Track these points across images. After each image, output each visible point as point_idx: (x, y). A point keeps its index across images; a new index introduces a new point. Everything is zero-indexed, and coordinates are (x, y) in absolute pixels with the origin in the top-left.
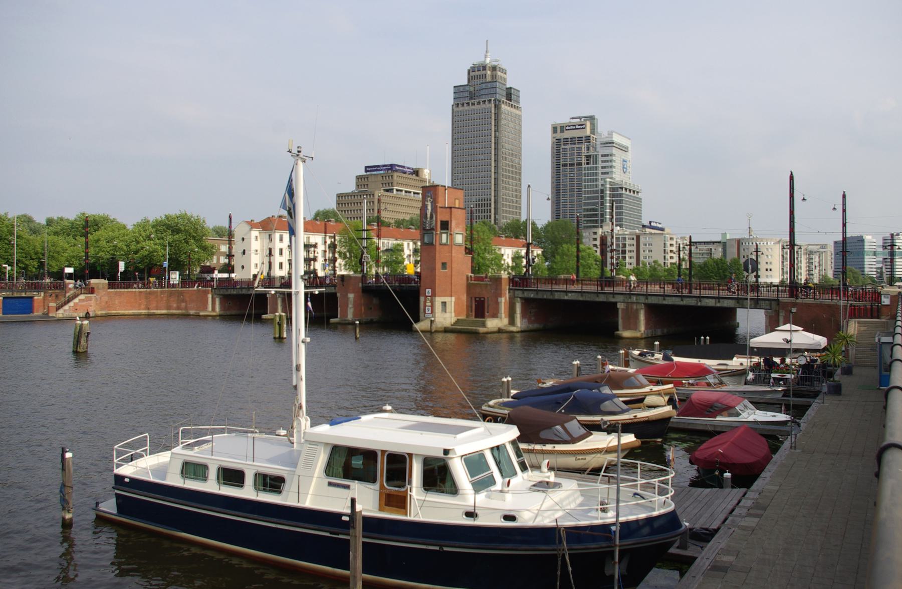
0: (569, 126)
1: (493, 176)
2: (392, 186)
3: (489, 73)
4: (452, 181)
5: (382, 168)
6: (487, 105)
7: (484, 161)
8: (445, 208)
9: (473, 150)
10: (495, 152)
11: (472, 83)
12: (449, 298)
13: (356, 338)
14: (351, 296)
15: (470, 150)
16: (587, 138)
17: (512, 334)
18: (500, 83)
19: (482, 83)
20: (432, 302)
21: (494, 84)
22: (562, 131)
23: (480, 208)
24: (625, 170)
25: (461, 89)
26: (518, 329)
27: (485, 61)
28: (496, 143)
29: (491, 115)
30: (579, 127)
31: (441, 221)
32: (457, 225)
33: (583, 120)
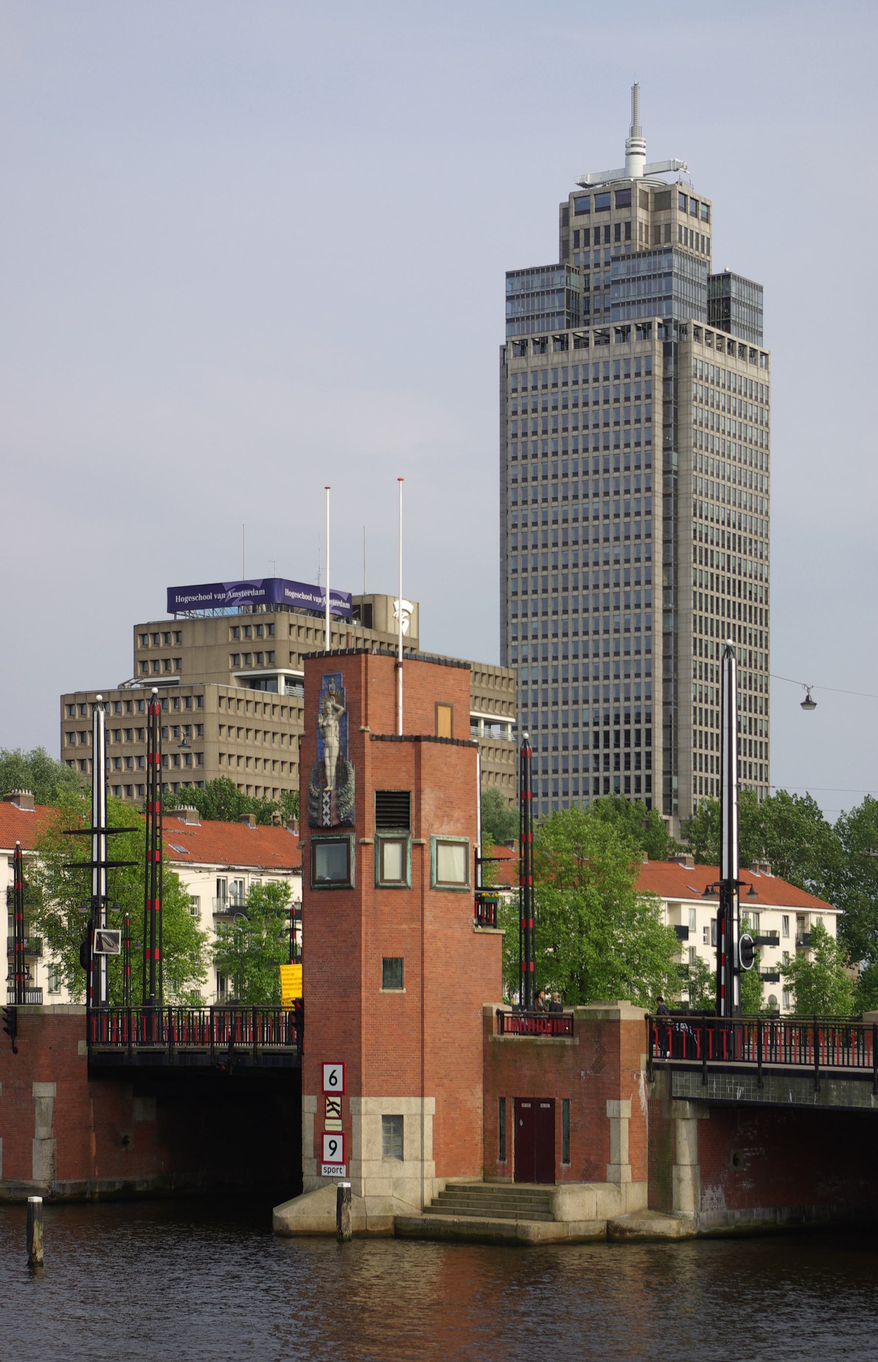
2: (273, 663)
3: (642, 216)
4: (504, 646)
5: (231, 595)
6: (636, 346)
8: (395, 739)
9: (581, 523)
10: (666, 531)
11: (579, 257)
12: (416, 1101)
13: (33, 1265)
14: (45, 1091)
15: (571, 525)
18: (683, 255)
19: (616, 259)
20: (347, 1116)
21: (663, 259)
25: (537, 283)
27: (627, 170)
28: (671, 496)
29: (650, 385)
32: (445, 808)
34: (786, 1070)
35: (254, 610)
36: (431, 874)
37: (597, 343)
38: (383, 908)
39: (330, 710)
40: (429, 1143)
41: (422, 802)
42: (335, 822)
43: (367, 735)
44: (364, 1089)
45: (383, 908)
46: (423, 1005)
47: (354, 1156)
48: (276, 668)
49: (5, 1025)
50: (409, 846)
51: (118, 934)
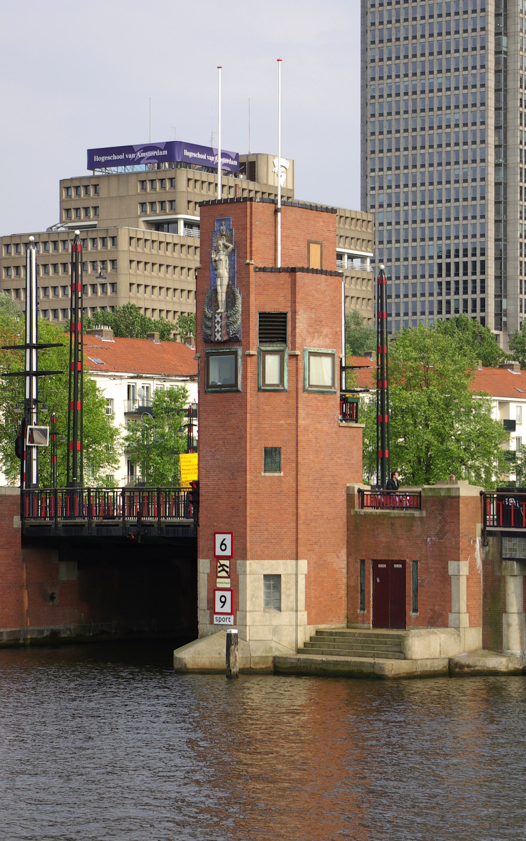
1: (491, 178)
4: (364, 195)
5: (139, 155)
7: (462, 129)
8: (275, 270)
10: (497, 100)
17: (492, 679)
23: (452, 279)
26: (515, 665)
31: (263, 315)
35: (159, 167)
36: (304, 379)
38: (264, 407)
39: (221, 248)
41: (297, 321)
42: (225, 338)
43: (251, 268)
44: (249, 553)
45: (264, 407)
46: (297, 485)
47: (240, 608)
48: (176, 214)
50: (286, 357)
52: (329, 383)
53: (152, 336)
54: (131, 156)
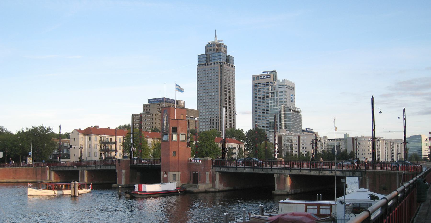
0: (262, 77)
8: (175, 119)
14: (124, 171)
16: (272, 83)
21: (220, 54)
22: (258, 79)
24: (292, 100)
25: (202, 57)
30: (267, 77)
33: (269, 73)
34: (298, 169)
37: (210, 65)
39: (165, 115)
40: (180, 178)
44: (170, 170)
47: (168, 180)
49: (118, 161)
50: (177, 135)
51: (79, 146)
52: (185, 140)
53: (158, 132)
54: (156, 100)
